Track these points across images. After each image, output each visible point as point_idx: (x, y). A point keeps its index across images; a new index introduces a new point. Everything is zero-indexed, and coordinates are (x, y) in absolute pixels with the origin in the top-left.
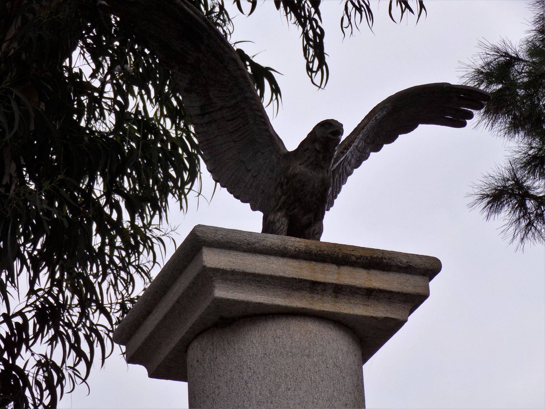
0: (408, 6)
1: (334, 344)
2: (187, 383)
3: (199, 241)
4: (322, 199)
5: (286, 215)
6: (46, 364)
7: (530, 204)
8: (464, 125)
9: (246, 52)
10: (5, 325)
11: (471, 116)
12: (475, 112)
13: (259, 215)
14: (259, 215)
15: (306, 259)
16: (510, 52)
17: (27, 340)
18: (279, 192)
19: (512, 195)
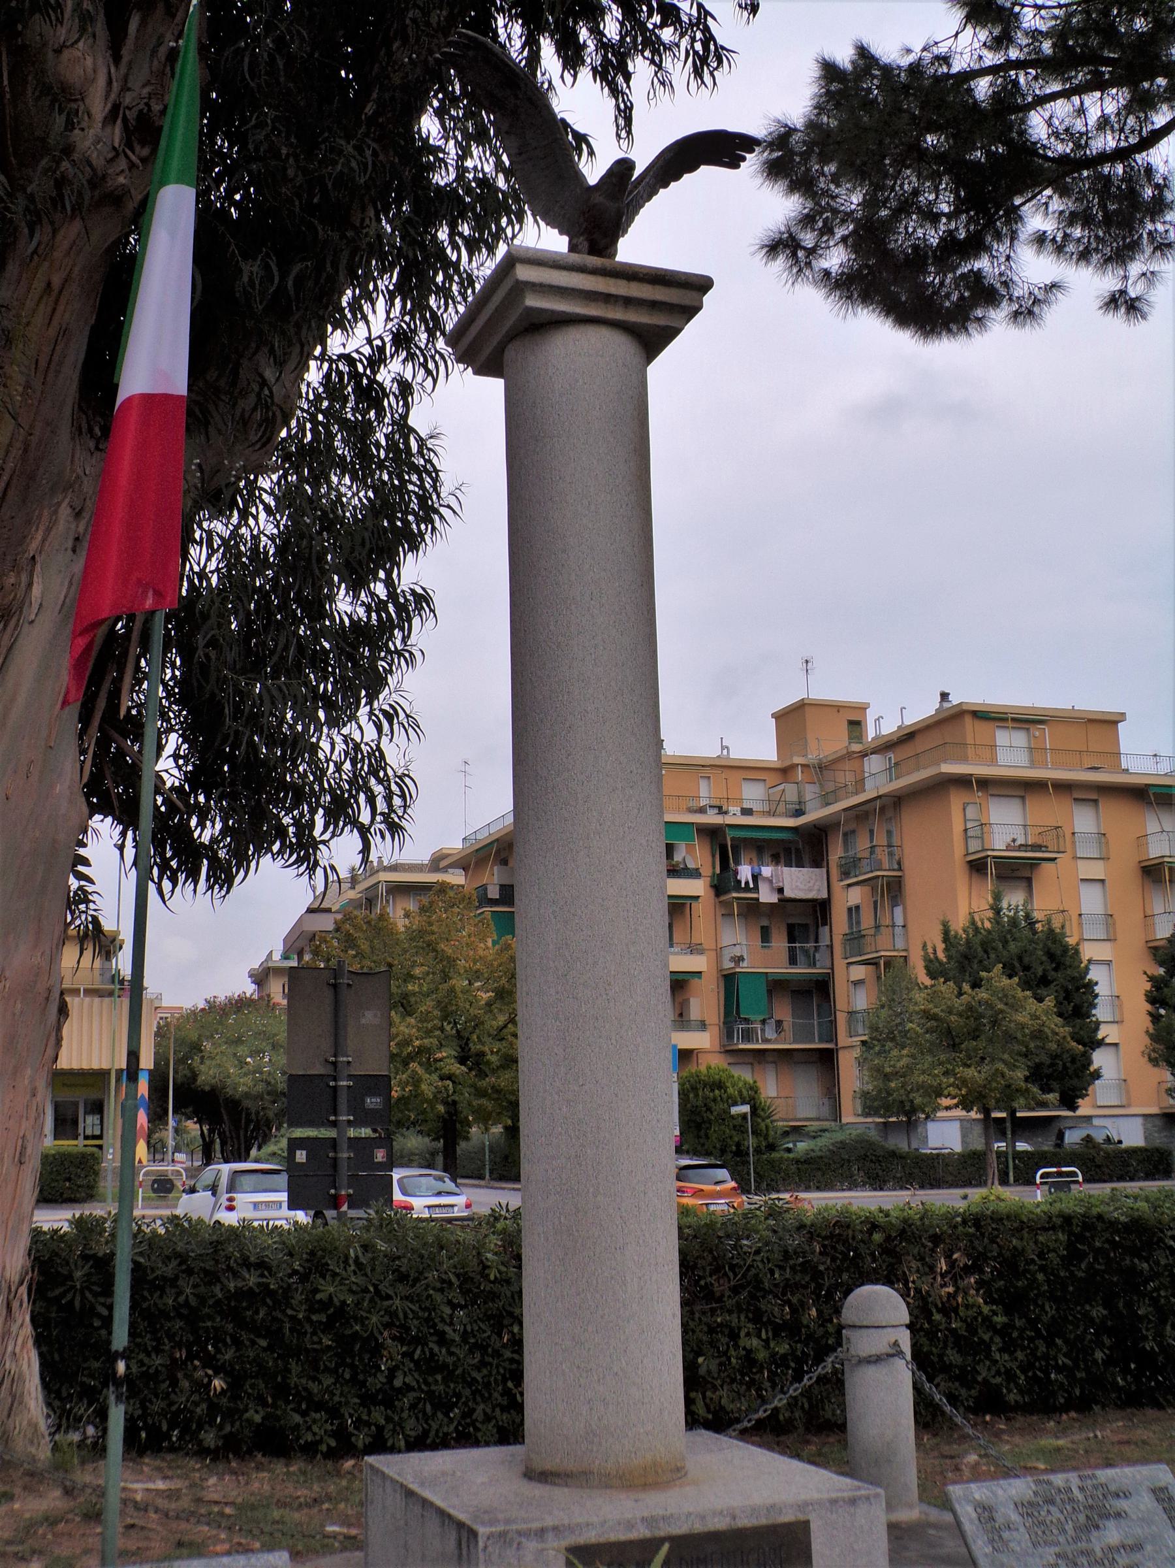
0: (703, 82)
1: (620, 346)
2: (502, 381)
5: (587, 239)
7: (800, 254)
8: (737, 166)
9: (568, 121)
10: (367, 347)
11: (744, 159)
12: (748, 156)
13: (565, 239)
14: (565, 239)
15: (601, 275)
16: (789, 123)
17: (386, 359)
18: (582, 220)
19: (786, 246)
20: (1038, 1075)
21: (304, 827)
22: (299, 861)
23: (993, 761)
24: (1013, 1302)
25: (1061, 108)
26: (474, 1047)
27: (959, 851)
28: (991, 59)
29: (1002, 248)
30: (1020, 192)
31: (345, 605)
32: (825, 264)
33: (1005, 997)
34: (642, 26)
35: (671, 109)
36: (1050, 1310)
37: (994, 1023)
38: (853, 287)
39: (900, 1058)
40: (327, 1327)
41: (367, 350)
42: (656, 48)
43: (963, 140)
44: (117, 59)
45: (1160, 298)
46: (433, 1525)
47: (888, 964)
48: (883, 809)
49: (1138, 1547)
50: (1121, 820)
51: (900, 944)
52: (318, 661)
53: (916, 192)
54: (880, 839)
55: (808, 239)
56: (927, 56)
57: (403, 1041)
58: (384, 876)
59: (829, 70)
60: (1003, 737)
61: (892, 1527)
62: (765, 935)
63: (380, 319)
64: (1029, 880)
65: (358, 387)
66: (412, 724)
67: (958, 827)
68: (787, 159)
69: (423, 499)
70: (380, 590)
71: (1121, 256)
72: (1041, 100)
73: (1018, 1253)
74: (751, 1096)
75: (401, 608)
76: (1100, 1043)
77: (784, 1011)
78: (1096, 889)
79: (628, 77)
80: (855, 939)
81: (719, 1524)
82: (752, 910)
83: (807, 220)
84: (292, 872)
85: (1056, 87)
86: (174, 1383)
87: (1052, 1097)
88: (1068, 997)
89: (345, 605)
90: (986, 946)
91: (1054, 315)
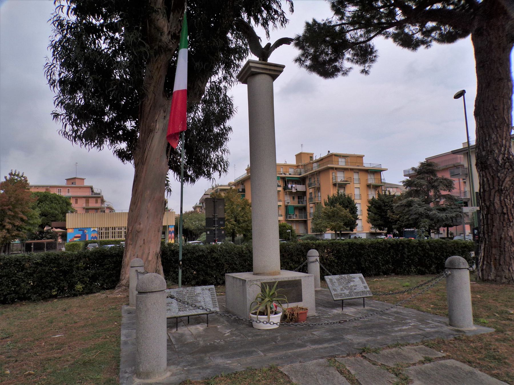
1: (268, 78)
2: (246, 85)
3: (249, 62)
4: (268, 56)
6: (225, 87)
20: (345, 224)
21: (209, 171)
22: (208, 177)
23: (338, 164)
24: (339, 258)
25: (352, 33)
26: (238, 219)
27: (331, 182)
28: (339, 22)
29: (340, 61)
30: (344, 49)
31: (216, 130)
32: (306, 64)
33: (339, 209)
34: (271, 15)
35: (277, 32)
36: (345, 259)
37: (337, 214)
38: (312, 68)
39: (319, 221)
40: (215, 262)
41: (218, 80)
42: (273, 19)
43: (333, 39)
44: (169, 22)
45: (372, 71)
46: (238, 281)
47: (317, 203)
48: (317, 174)
49: (356, 286)
50: (363, 176)
51: (319, 200)
52: (211, 140)
53: (324, 49)
54: (316, 180)
55: (303, 59)
56: (327, 22)
57: (227, 213)
58: (219, 187)
59: (308, 24)
60: (340, 160)
61: (315, 291)
62: (294, 198)
63: (221, 73)
64: (345, 188)
65: (216, 88)
66: (228, 152)
67: (331, 177)
68: (299, 42)
69: (230, 110)
70: (222, 127)
71: (364, 62)
72: (348, 31)
73: (340, 249)
74: (291, 229)
75: (226, 130)
76: (358, 219)
77: (297, 213)
78: (358, 189)
79: (268, 25)
80: (311, 199)
81: (286, 280)
82: (291, 193)
83: (303, 55)
84: (206, 179)
85: (352, 28)
86: (187, 273)
87: (348, 228)
88: (352, 210)
89: (216, 130)
90: (336, 200)
91: (350, 74)
